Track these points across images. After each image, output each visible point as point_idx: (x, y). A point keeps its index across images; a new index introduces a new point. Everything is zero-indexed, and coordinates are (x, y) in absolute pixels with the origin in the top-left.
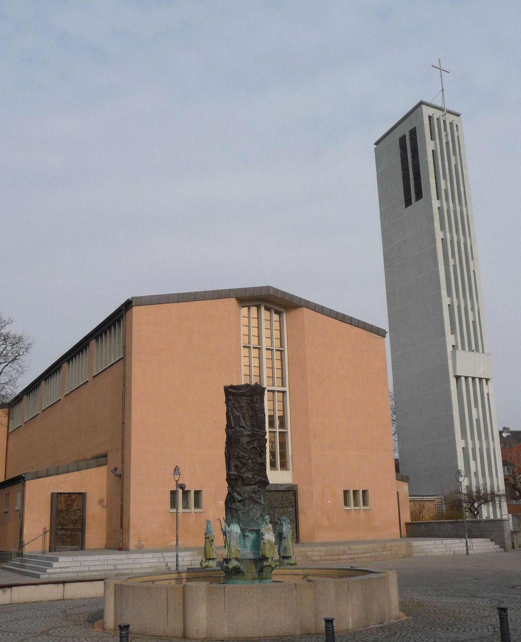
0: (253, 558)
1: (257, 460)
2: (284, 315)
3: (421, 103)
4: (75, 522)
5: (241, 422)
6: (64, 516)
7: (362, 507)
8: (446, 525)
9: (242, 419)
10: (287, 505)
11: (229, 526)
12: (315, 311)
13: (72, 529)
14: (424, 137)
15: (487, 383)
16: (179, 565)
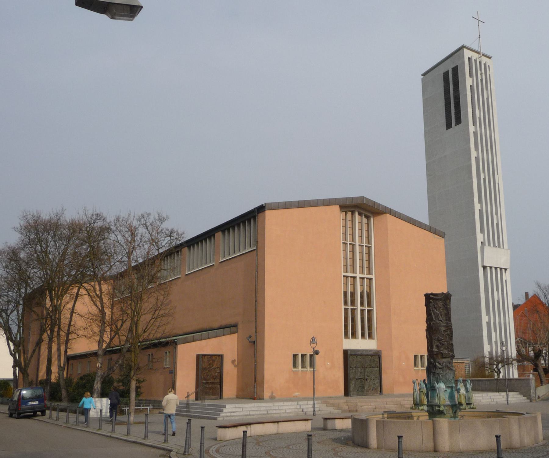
0: (450, 404)
1: (449, 342)
2: (372, 219)
3: (463, 47)
4: (214, 378)
9: (440, 315)
10: (374, 366)
15: (505, 273)
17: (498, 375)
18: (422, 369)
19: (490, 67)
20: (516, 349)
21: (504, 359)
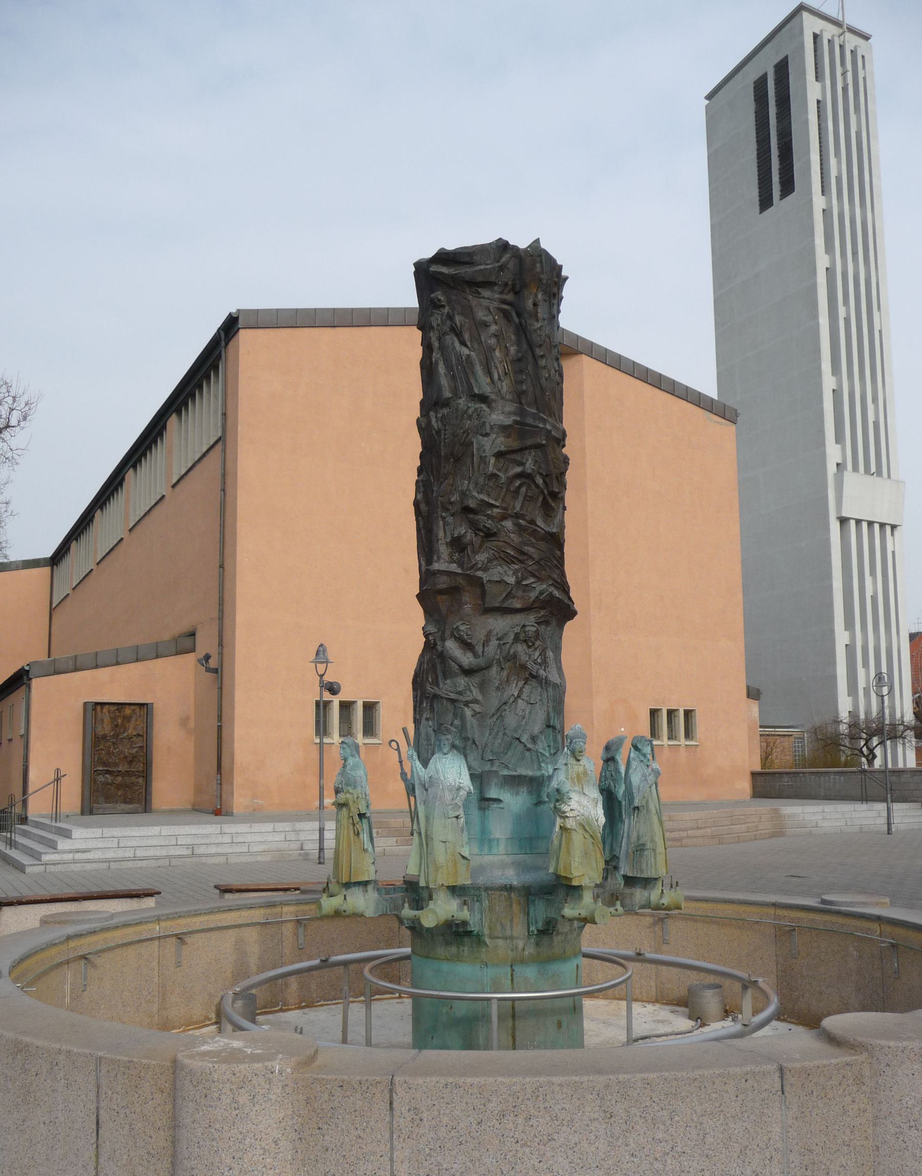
1: (533, 522)
5: (476, 380)
6: (110, 747)
7: (683, 741)
8: (832, 777)
9: (479, 370)
11: (425, 763)
12: (605, 363)
13: (126, 771)
14: (803, 73)
15: (892, 534)
16: (325, 848)
17: (870, 762)
18: (688, 743)
19: (866, 58)
20: (914, 708)
21: (883, 727)
